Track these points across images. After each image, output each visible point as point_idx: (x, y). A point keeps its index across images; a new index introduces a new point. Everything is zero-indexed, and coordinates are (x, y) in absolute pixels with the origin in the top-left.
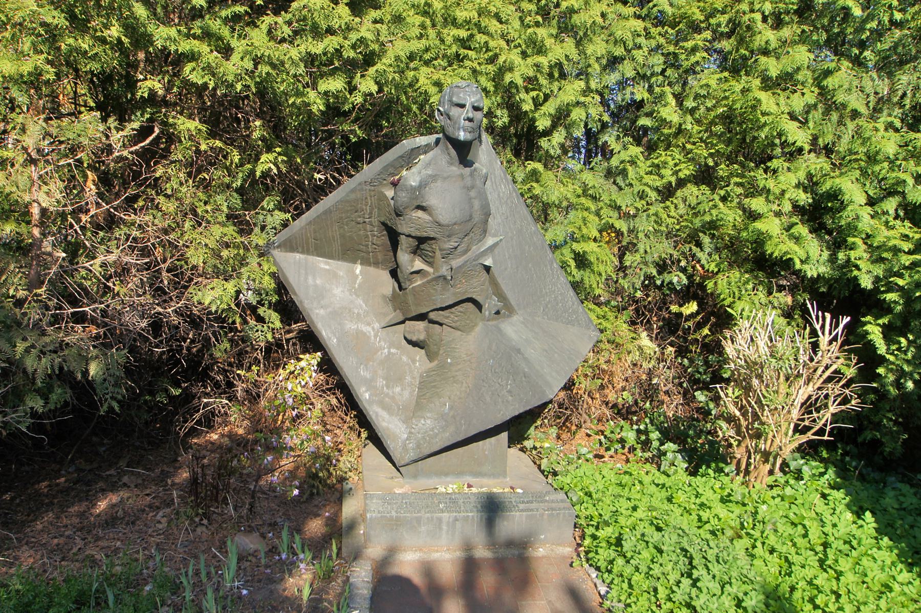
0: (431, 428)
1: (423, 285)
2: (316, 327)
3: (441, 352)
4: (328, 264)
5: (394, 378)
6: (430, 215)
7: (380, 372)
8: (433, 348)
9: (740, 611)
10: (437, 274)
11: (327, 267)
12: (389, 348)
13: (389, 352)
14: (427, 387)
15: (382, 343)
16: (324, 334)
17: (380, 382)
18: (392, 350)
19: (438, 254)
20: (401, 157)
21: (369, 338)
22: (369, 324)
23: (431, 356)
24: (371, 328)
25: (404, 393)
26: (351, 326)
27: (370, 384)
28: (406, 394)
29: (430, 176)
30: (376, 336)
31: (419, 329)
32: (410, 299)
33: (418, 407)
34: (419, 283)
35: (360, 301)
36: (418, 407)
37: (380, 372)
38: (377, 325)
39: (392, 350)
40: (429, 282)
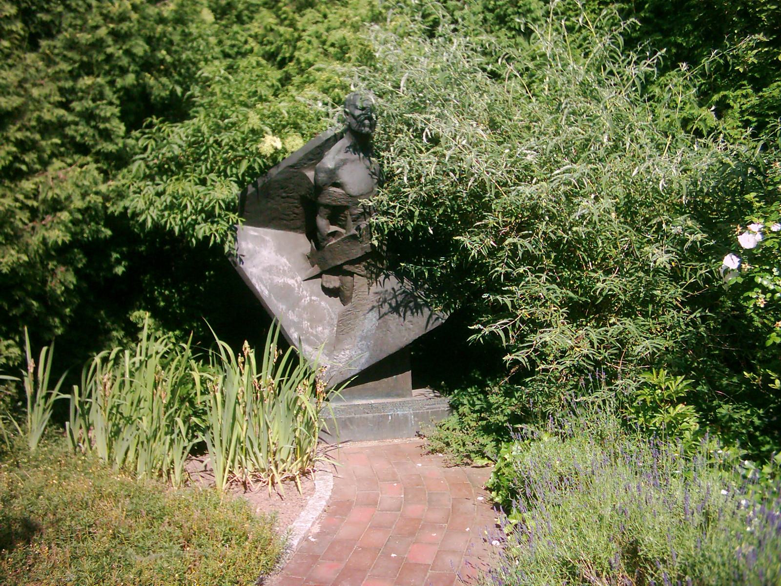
0: (354, 356)
1: (338, 243)
2: (251, 282)
3: (354, 295)
4: (255, 231)
5: (315, 321)
6: (343, 189)
7: (305, 316)
8: (348, 293)
9: (576, 584)
10: (349, 234)
11: (256, 234)
12: (311, 296)
13: (311, 300)
14: (344, 326)
15: (305, 292)
16: (257, 287)
17: (306, 324)
18: (314, 298)
19: (349, 218)
20: (318, 147)
21: (293, 289)
22: (293, 278)
23: (344, 302)
24: (295, 281)
25: (325, 332)
26: (280, 280)
27: (299, 328)
28: (327, 331)
29: (342, 160)
30: (299, 287)
31: (333, 282)
32: (328, 255)
33: (334, 346)
34: (334, 241)
35: (284, 260)
36: (334, 346)
37: (305, 316)
38: (299, 279)
39: (314, 298)
40: (343, 240)
